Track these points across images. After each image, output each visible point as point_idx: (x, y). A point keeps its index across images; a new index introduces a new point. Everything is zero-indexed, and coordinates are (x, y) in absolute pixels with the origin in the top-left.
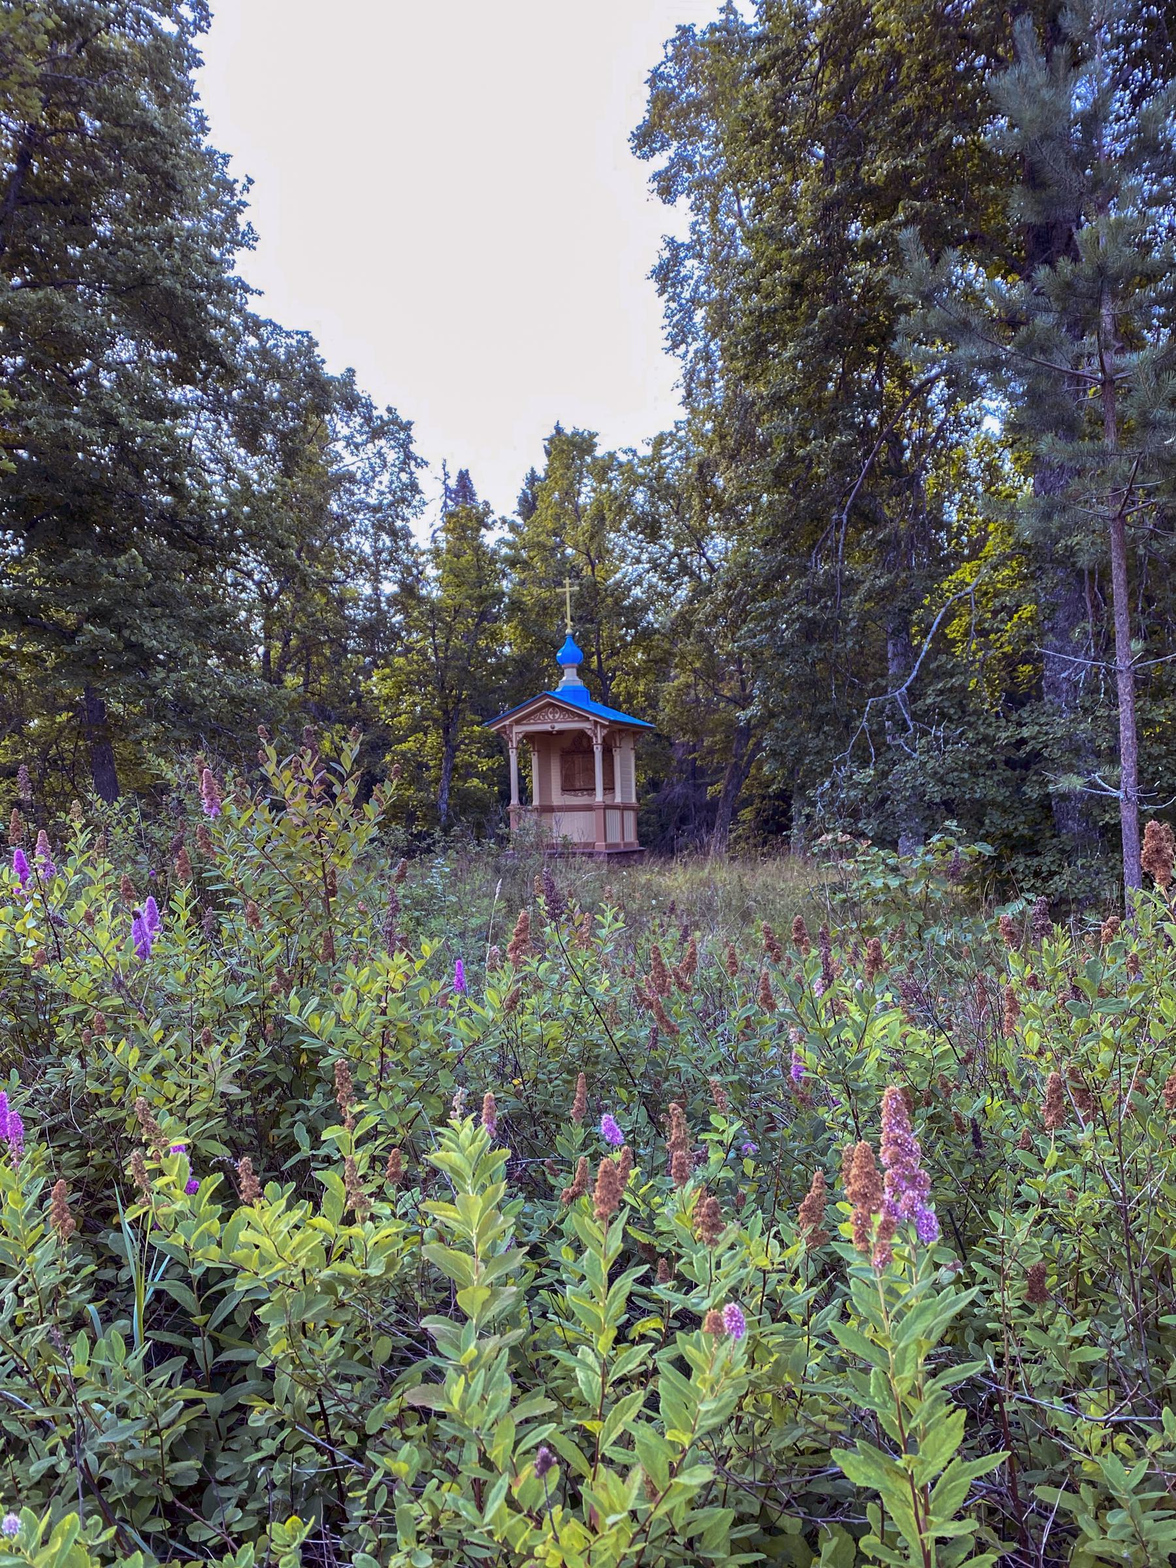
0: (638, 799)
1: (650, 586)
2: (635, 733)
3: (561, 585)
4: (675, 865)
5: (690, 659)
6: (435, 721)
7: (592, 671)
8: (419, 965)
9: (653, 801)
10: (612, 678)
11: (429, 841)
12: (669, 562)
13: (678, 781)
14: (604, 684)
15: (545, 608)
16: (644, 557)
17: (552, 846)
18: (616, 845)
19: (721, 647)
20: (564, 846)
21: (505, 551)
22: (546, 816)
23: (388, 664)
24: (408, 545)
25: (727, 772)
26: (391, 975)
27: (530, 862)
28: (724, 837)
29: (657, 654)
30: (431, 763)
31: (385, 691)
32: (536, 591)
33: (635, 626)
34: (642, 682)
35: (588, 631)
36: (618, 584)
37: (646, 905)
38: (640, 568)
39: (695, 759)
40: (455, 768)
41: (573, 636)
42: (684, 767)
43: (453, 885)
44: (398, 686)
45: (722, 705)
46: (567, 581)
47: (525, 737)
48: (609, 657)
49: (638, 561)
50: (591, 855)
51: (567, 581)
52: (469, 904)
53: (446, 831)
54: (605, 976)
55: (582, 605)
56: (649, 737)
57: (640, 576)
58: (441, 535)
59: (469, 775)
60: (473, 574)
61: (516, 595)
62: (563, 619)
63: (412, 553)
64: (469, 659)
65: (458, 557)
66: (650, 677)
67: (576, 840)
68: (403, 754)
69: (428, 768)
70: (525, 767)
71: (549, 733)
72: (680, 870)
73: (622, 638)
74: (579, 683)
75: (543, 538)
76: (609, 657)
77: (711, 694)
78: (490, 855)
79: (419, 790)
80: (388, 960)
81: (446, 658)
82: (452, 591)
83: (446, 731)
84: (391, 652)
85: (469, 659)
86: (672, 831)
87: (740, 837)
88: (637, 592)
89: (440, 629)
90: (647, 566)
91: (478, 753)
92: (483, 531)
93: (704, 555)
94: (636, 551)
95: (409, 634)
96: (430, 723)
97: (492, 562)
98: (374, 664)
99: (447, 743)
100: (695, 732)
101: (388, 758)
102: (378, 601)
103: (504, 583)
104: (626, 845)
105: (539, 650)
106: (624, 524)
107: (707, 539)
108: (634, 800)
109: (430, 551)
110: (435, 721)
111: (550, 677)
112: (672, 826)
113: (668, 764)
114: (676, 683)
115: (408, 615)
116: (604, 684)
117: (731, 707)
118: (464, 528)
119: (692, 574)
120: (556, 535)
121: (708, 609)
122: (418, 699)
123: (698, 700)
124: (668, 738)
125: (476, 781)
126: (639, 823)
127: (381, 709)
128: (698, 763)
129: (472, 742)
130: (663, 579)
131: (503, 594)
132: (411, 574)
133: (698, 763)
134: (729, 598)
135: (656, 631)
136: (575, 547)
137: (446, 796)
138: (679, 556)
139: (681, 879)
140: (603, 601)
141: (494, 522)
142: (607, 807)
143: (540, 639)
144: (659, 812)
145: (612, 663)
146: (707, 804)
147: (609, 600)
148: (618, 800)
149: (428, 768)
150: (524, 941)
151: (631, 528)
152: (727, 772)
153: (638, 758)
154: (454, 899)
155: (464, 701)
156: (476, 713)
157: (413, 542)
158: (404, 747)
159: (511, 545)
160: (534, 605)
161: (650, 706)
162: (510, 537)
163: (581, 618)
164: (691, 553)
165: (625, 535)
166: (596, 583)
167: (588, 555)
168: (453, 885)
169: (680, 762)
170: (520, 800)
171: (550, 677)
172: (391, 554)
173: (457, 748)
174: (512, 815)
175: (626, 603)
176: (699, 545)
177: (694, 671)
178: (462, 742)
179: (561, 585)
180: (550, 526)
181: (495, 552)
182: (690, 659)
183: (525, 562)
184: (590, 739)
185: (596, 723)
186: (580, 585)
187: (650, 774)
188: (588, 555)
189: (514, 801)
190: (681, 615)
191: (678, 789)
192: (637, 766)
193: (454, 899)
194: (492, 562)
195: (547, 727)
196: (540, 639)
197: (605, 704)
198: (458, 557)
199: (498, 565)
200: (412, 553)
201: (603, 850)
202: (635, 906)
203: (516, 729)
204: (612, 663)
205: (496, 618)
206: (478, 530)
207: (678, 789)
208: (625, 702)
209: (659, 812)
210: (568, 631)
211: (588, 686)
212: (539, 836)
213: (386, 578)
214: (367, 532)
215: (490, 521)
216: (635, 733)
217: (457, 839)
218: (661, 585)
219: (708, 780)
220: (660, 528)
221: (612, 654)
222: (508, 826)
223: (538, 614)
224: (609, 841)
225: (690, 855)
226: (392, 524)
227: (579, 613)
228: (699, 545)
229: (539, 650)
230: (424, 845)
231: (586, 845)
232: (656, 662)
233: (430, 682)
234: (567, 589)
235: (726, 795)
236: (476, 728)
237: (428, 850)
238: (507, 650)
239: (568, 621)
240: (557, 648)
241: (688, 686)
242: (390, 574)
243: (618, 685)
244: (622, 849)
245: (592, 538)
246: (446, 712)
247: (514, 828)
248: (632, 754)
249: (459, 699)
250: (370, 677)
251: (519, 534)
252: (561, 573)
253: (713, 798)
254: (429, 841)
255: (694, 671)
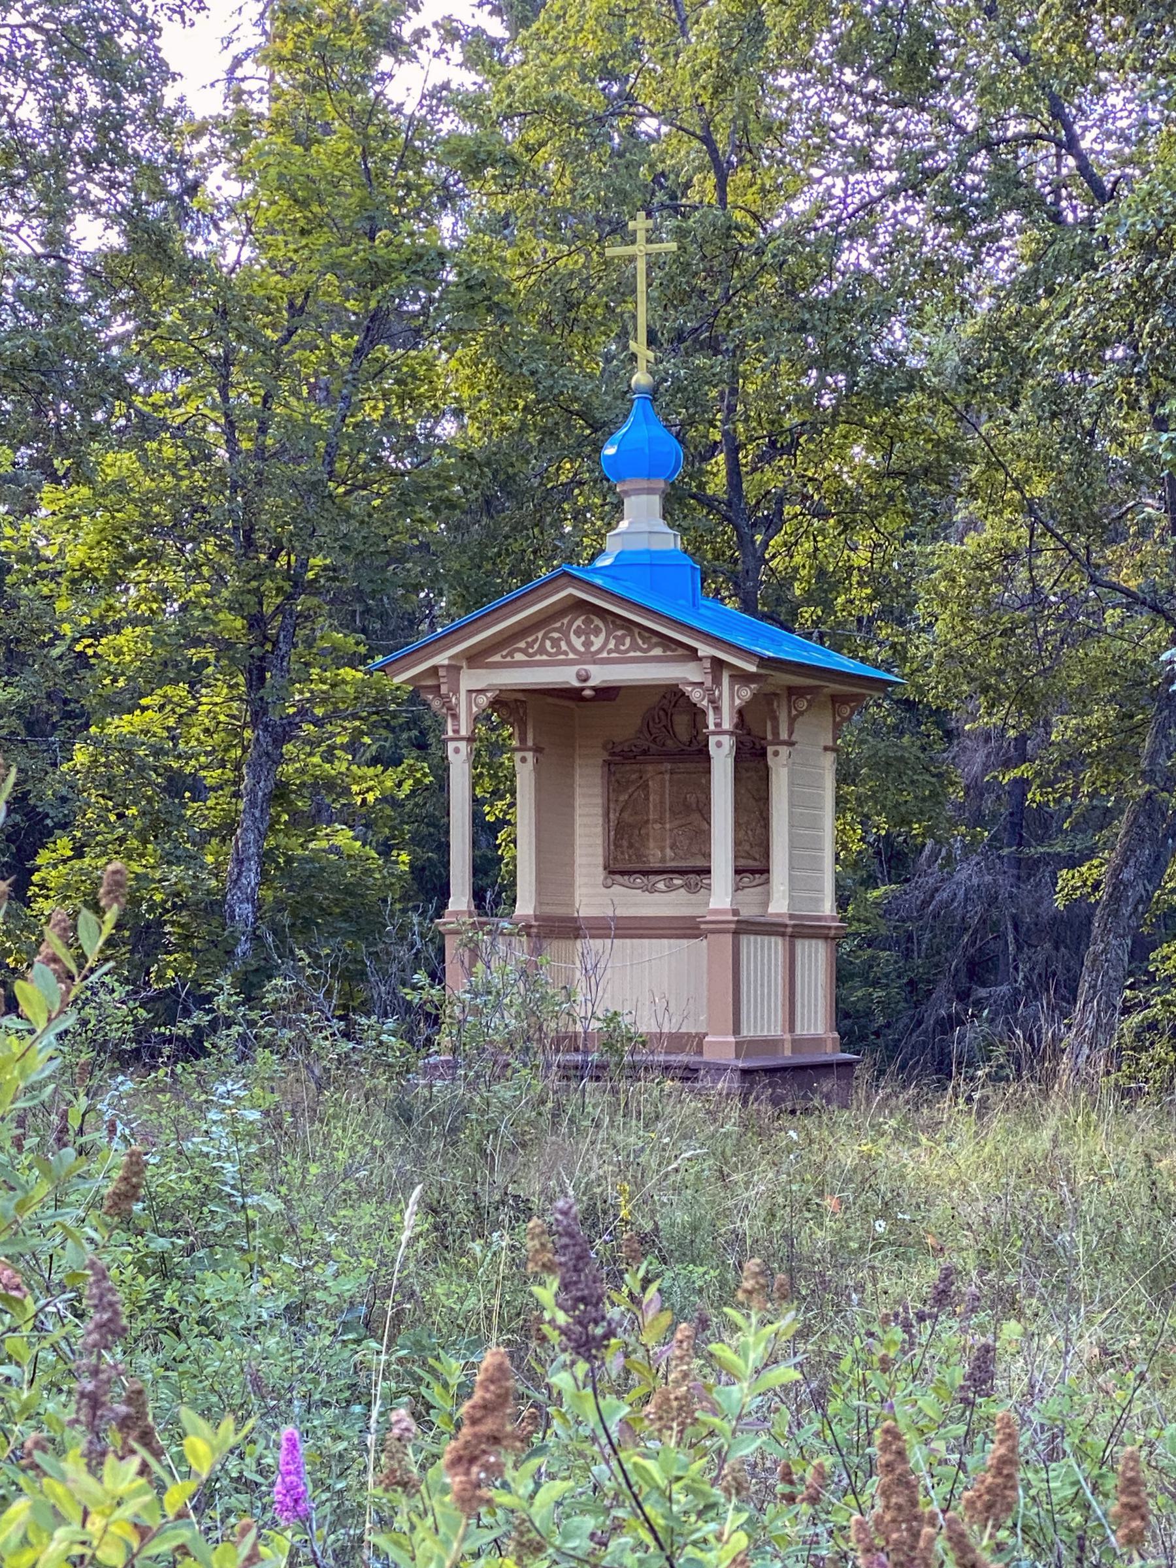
0: (842, 902)
1: (899, 242)
2: (837, 700)
3: (618, 229)
4: (948, 1108)
5: (1017, 469)
6: (225, 647)
7: (709, 503)
8: (178, 1494)
9: (887, 910)
10: (773, 524)
11: (200, 1018)
12: (963, 166)
13: (968, 849)
14: (744, 542)
15: (571, 306)
16: (884, 148)
17: (570, 1042)
18: (771, 1044)
19: (1116, 435)
20: (610, 1045)
21: (449, 124)
22: (554, 947)
23: (81, 474)
24: (155, 104)
25: (1121, 825)
26: (96, 1523)
27: (504, 1091)
28: (1104, 1028)
29: (918, 452)
30: (211, 777)
31: (76, 555)
32: (540, 248)
33: (850, 365)
34: (864, 538)
35: (702, 378)
36: (796, 231)
37: (856, 1232)
38: (868, 183)
39: (1022, 784)
40: (280, 793)
41: (654, 393)
42: (988, 804)
43: (270, 1156)
44: (114, 537)
45: (1112, 616)
46: (640, 224)
47: (497, 703)
48: (764, 458)
49: (866, 161)
50: (689, 1074)
51: (640, 224)
52: (317, 1218)
53: (249, 989)
54: (733, 1519)
55: (685, 297)
56: (881, 711)
57: (867, 206)
58: (254, 75)
59: (319, 816)
60: (351, 196)
61: (480, 261)
62: (624, 336)
63: (167, 126)
64: (330, 455)
65: (307, 143)
66: (891, 523)
67: (646, 1025)
68: (126, 746)
69: (199, 791)
70: (496, 794)
71: (571, 694)
72: (966, 1127)
73: (806, 400)
74: (669, 541)
75: (571, 86)
76: (764, 458)
77: (1079, 581)
78: (380, 1062)
79: (170, 859)
80: (88, 1481)
81: (260, 453)
82: (284, 246)
83: (256, 678)
84: (95, 432)
85: (330, 455)
86: (943, 1006)
87: (1152, 1026)
88: (856, 255)
89: (247, 366)
90: (891, 177)
91: (352, 747)
92: (386, 63)
93: (1071, 145)
94: (856, 131)
95: (151, 377)
96: (208, 653)
97: (411, 157)
98: (43, 465)
99: (259, 714)
100: (1025, 698)
101: (81, 756)
102: (61, 275)
103: (446, 221)
104: (797, 1044)
105: (548, 433)
106: (823, 44)
107: (1084, 97)
108: (828, 907)
109: (220, 122)
110: (225, 647)
111: (578, 516)
112: (941, 989)
113: (936, 797)
114: (971, 543)
115: (149, 323)
116: (744, 542)
117: (1143, 620)
118: (325, 52)
119: (1029, 204)
120: (610, 75)
121: (1079, 319)
122: (171, 577)
123: (1037, 596)
124: (939, 715)
125: (344, 837)
126: (842, 975)
127: (61, 605)
128: (1034, 796)
129: (335, 714)
130: (939, 219)
131: (442, 255)
132: (160, 194)
133: (1034, 796)
134: (1146, 284)
135: (913, 381)
136: (668, 114)
137: (251, 878)
138: (989, 146)
139: (966, 1156)
140: (749, 285)
141: (420, 34)
142: (744, 928)
143: (550, 398)
144: (906, 944)
145: (771, 478)
146: (1056, 919)
147: (770, 282)
148: (779, 906)
149: (199, 791)
150: (495, 1439)
151: (843, 61)
152: (1121, 825)
153: (845, 776)
154: (274, 1205)
155: (312, 588)
156: (347, 625)
157: (170, 96)
158: (121, 725)
159: (469, 106)
160: (535, 293)
161: (886, 613)
162: (467, 80)
163: (680, 337)
164: (1030, 139)
165: (825, 77)
166: (731, 228)
167: (707, 140)
168: (270, 1156)
169: (976, 789)
170: (478, 895)
171: (578, 516)
172: (101, 131)
173: (284, 732)
174: (451, 944)
175: (821, 291)
176: (1057, 113)
177: (1029, 508)
178: (303, 712)
179: (618, 229)
180: (592, 51)
181: (417, 125)
182: (1017, 469)
183: (511, 161)
184: (697, 714)
185: (718, 664)
186: (680, 234)
187: (882, 824)
188: (707, 140)
189: (460, 900)
190: (993, 333)
191: (965, 873)
192: (840, 801)
193: (274, 1205)
194: (411, 157)
195: (566, 676)
196: (550, 398)
197: (748, 606)
198: (307, 143)
199: (429, 170)
200: (167, 126)
201: (728, 1057)
202: (823, 1237)
203: (470, 679)
204: (771, 478)
205: (415, 336)
206: (369, 60)
207: (965, 873)
208: (809, 599)
209: (906, 944)
210: (641, 378)
211: (694, 549)
212: (530, 1012)
213: (89, 204)
214: (31, 65)
215: (406, 32)
216: (837, 700)
217: (281, 1016)
218: (935, 237)
219: (1060, 847)
220: (934, 58)
221: (774, 449)
222: (437, 977)
223: (546, 321)
224: (747, 1032)
225: (995, 1078)
226: (106, 40)
227: (678, 319)
228: (1057, 113)
229: (548, 433)
230: (183, 1028)
231: (678, 1041)
232: (910, 478)
233: (209, 528)
234: (640, 248)
235: (1117, 897)
236: (347, 673)
237: (192, 1048)
238: (448, 428)
239: (639, 346)
240: (601, 428)
241: (1009, 555)
242: (96, 192)
243: (789, 547)
244: (787, 1056)
245: (721, 86)
246: (256, 622)
247: (457, 983)
248: (828, 762)
249: (297, 583)
250: (30, 510)
251: (496, 72)
252: (622, 197)
253: (1073, 904)
254: (200, 1018)
255: (1029, 508)
